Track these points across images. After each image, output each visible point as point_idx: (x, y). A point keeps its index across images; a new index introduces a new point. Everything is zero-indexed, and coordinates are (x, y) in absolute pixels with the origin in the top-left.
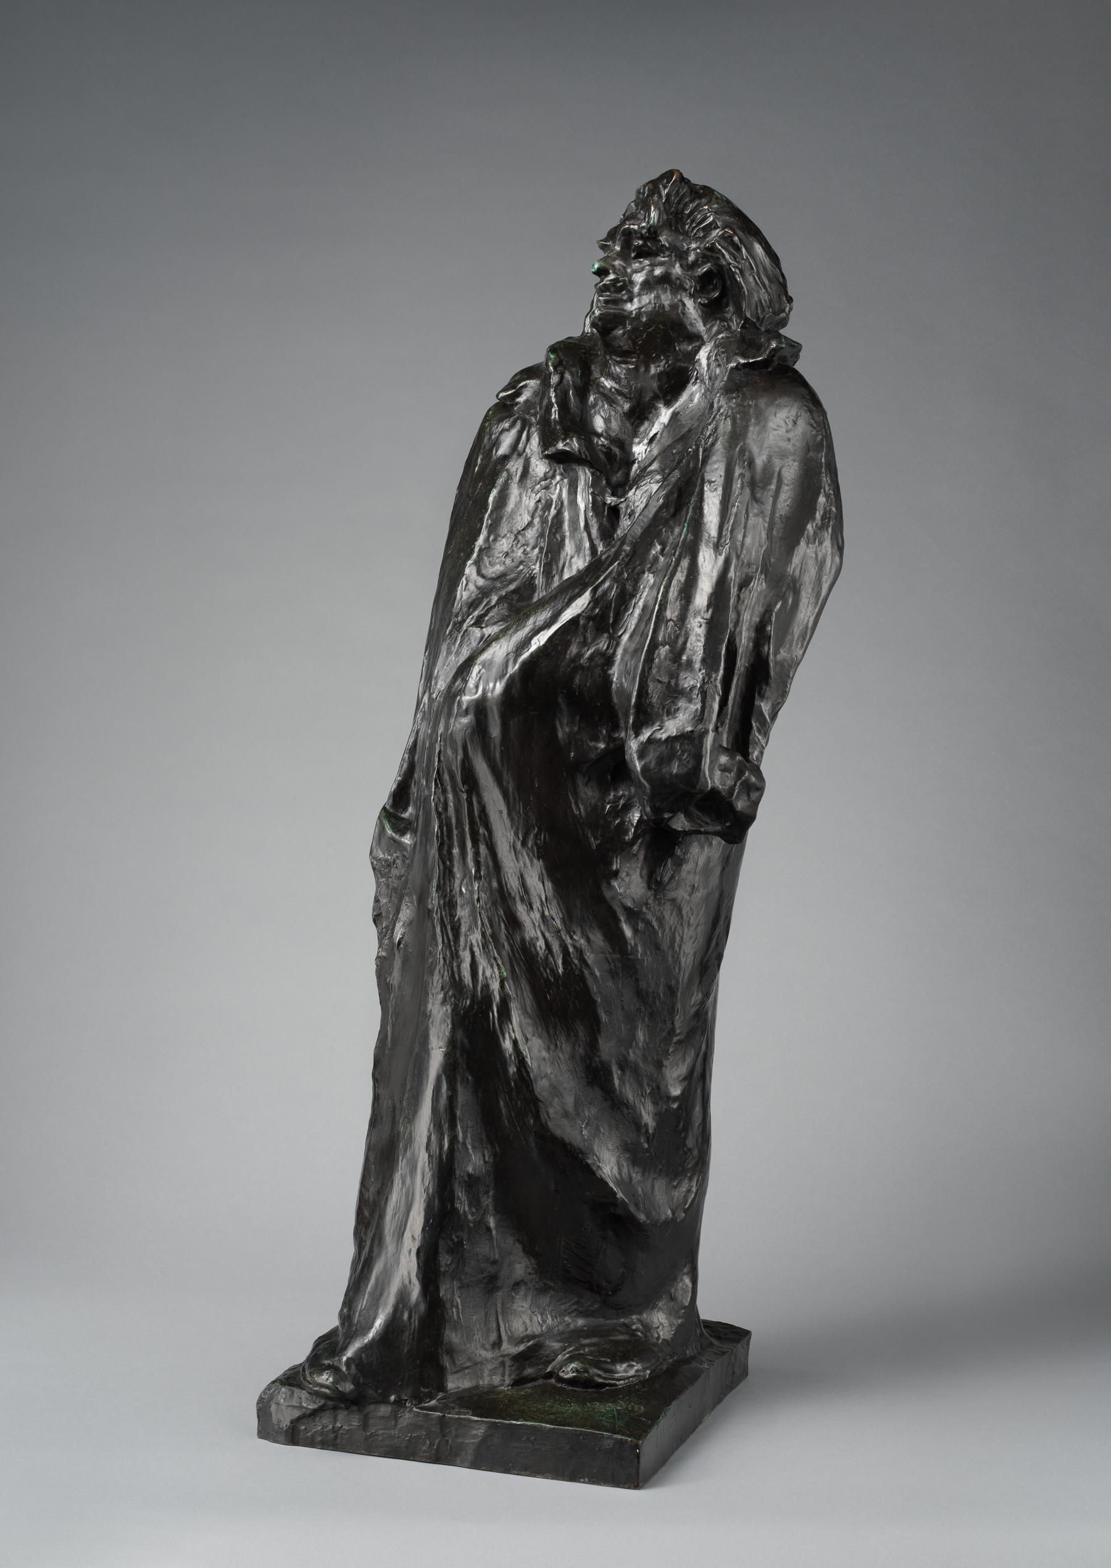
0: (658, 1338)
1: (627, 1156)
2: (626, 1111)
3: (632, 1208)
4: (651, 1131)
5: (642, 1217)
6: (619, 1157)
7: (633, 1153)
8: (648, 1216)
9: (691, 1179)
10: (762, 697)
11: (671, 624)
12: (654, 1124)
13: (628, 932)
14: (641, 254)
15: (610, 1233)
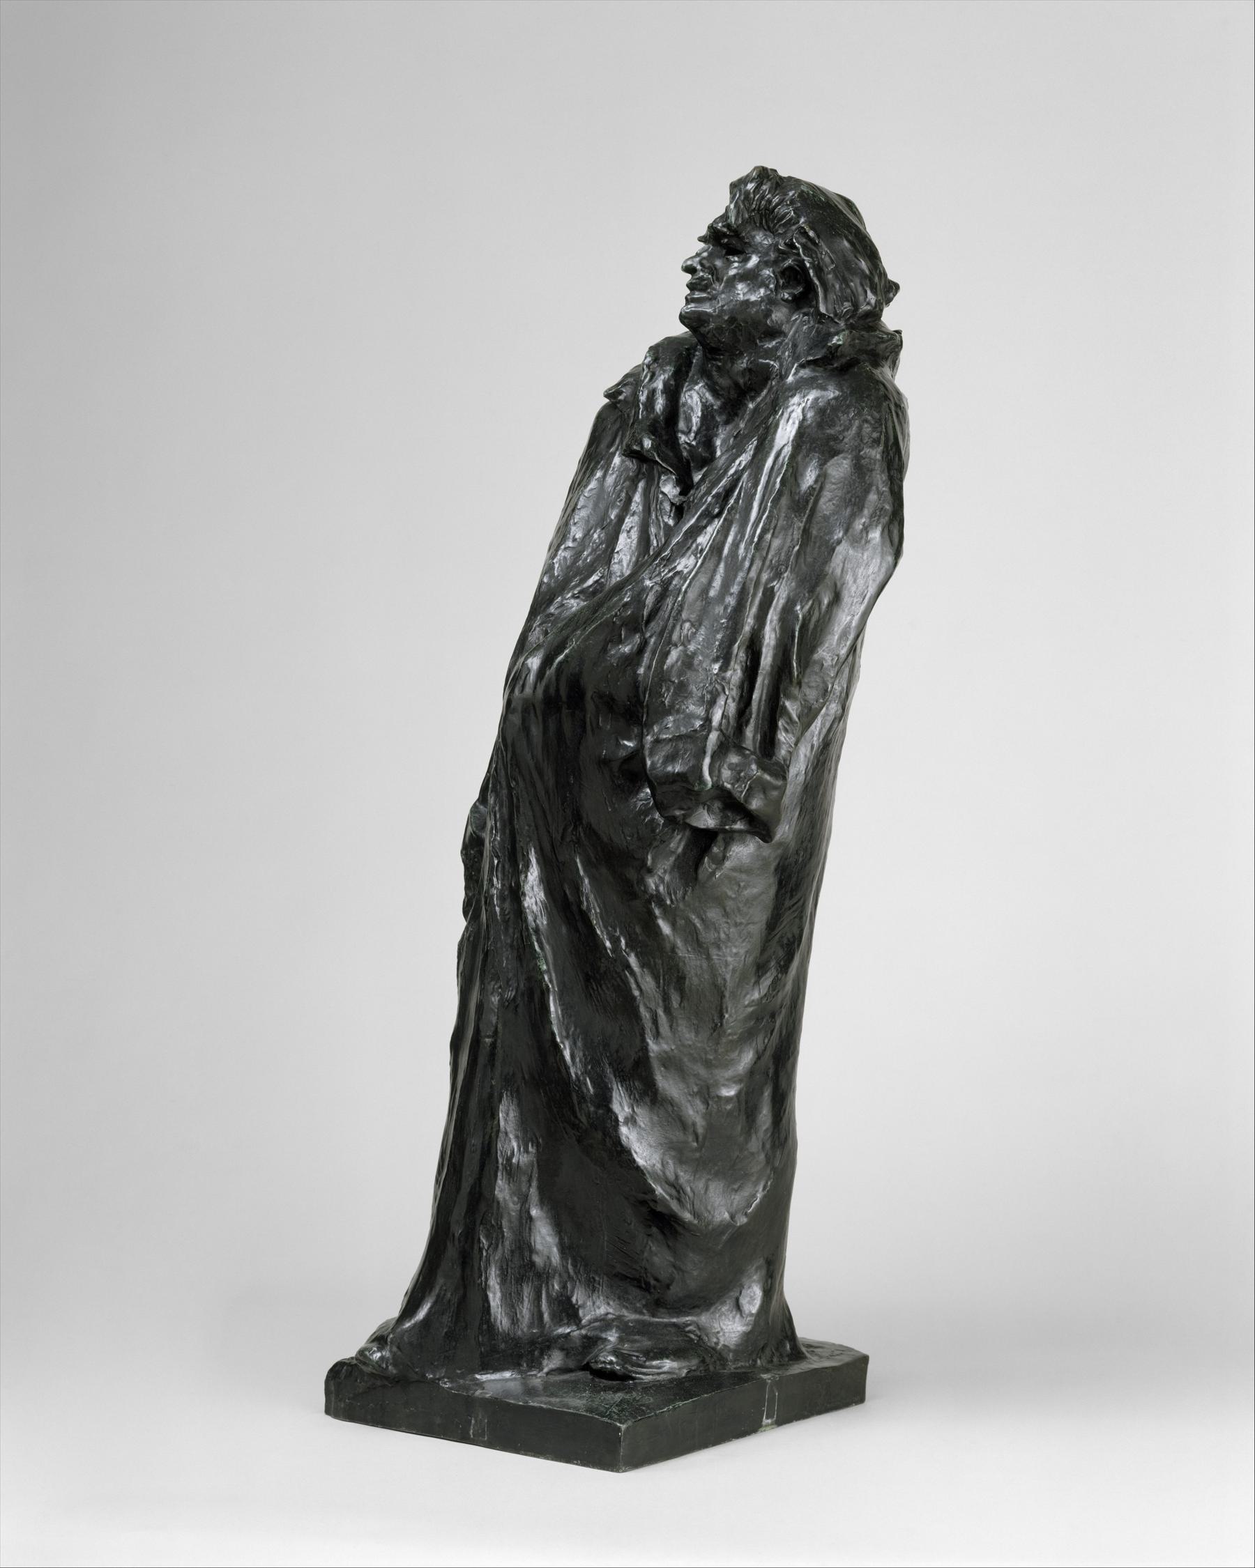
0: (717, 1344)
1: (673, 1153)
2: (670, 1109)
3: (674, 1206)
4: (700, 1131)
5: (687, 1216)
6: (664, 1154)
7: (677, 1151)
8: (695, 1214)
9: (756, 1184)
10: (788, 697)
11: (687, 625)
12: (704, 1123)
13: (665, 928)
14: (732, 251)
15: (654, 1230)
